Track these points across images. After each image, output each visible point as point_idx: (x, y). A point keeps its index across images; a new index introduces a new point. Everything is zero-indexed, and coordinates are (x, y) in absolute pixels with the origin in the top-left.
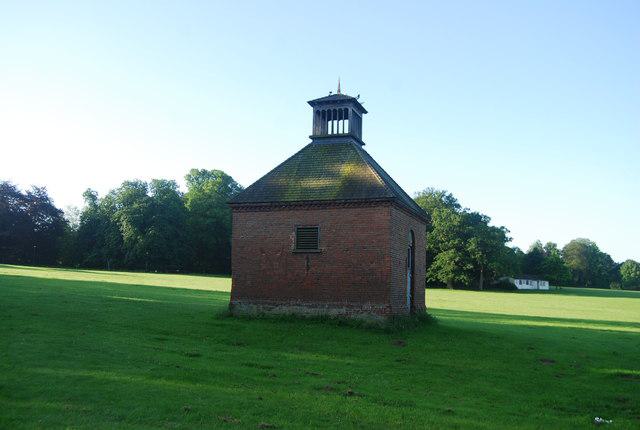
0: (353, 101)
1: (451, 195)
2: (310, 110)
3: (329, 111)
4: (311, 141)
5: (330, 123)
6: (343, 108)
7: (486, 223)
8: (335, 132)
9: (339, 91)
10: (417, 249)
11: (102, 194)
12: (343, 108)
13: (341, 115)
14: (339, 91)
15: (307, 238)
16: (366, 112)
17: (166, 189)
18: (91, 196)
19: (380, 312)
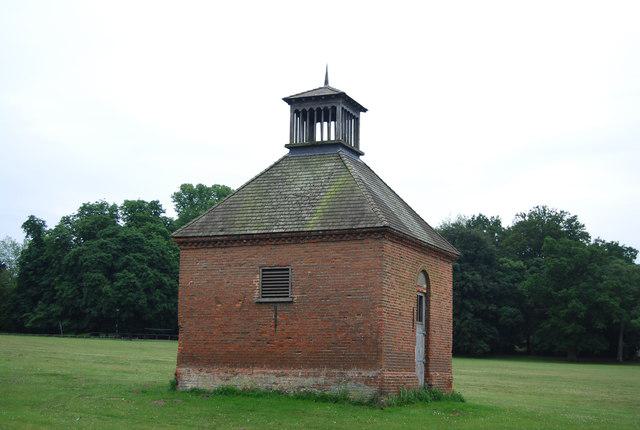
0: (342, 97)
1: (574, 218)
2: (287, 107)
3: (319, 110)
4: (288, 151)
5: (318, 125)
6: (329, 106)
7: (629, 261)
8: (325, 139)
9: (326, 82)
10: (434, 297)
11: (51, 224)
12: (329, 106)
13: (328, 116)
14: (326, 82)
15: (276, 280)
16: (365, 110)
17: (142, 213)
18: (33, 226)
19: (368, 381)
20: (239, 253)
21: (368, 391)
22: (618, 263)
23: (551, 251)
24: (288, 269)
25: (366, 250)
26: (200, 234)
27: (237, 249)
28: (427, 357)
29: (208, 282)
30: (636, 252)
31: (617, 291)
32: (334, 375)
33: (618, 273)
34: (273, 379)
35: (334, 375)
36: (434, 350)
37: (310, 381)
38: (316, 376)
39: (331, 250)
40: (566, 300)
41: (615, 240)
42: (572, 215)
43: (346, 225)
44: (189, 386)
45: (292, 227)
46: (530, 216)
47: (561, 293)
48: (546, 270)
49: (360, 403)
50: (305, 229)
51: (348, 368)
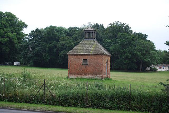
1: (127, 26)
15: (85, 61)
19: (100, 76)
20: (79, 57)
21: (100, 78)
22: (141, 41)
23: (120, 37)
25: (100, 57)
28: (107, 72)
31: (140, 50)
32: (95, 76)
33: (141, 44)
35: (95, 76)
36: (108, 72)
37: (91, 77)
38: (92, 76)
39: (94, 57)
40: (125, 53)
41: (141, 32)
42: (127, 24)
43: (97, 53)
44: (71, 78)
45: (88, 53)
46: (113, 25)
48: (118, 43)
49: (99, 80)
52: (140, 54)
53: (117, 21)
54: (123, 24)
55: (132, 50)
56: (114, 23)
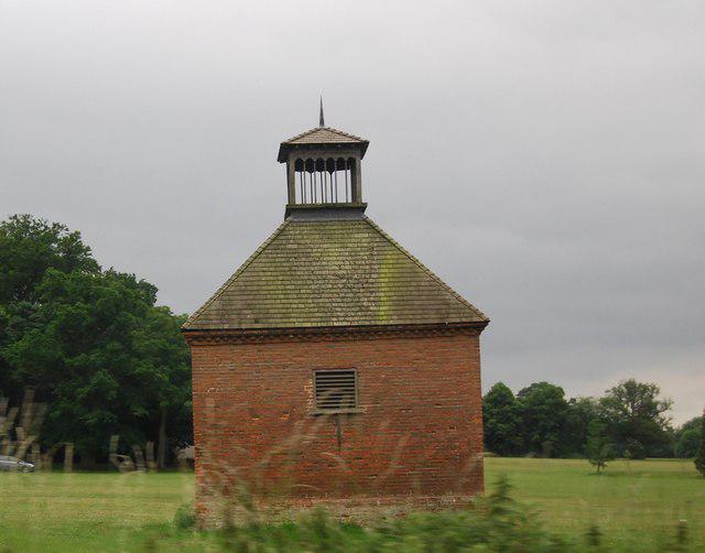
9: (322, 122)
14: (322, 122)
23: (58, 291)
24: (353, 373)
26: (226, 326)
27: (279, 346)
29: (238, 388)
30: (155, 290)
34: (342, 510)
39: (411, 348)
40: (85, 372)
42: (72, 231)
43: (433, 319)
45: (358, 320)
47: (79, 360)
50: (379, 323)
51: (441, 493)
52: (167, 379)
53: (20, 212)
54: (55, 225)
55: (123, 356)
56: (9, 221)
